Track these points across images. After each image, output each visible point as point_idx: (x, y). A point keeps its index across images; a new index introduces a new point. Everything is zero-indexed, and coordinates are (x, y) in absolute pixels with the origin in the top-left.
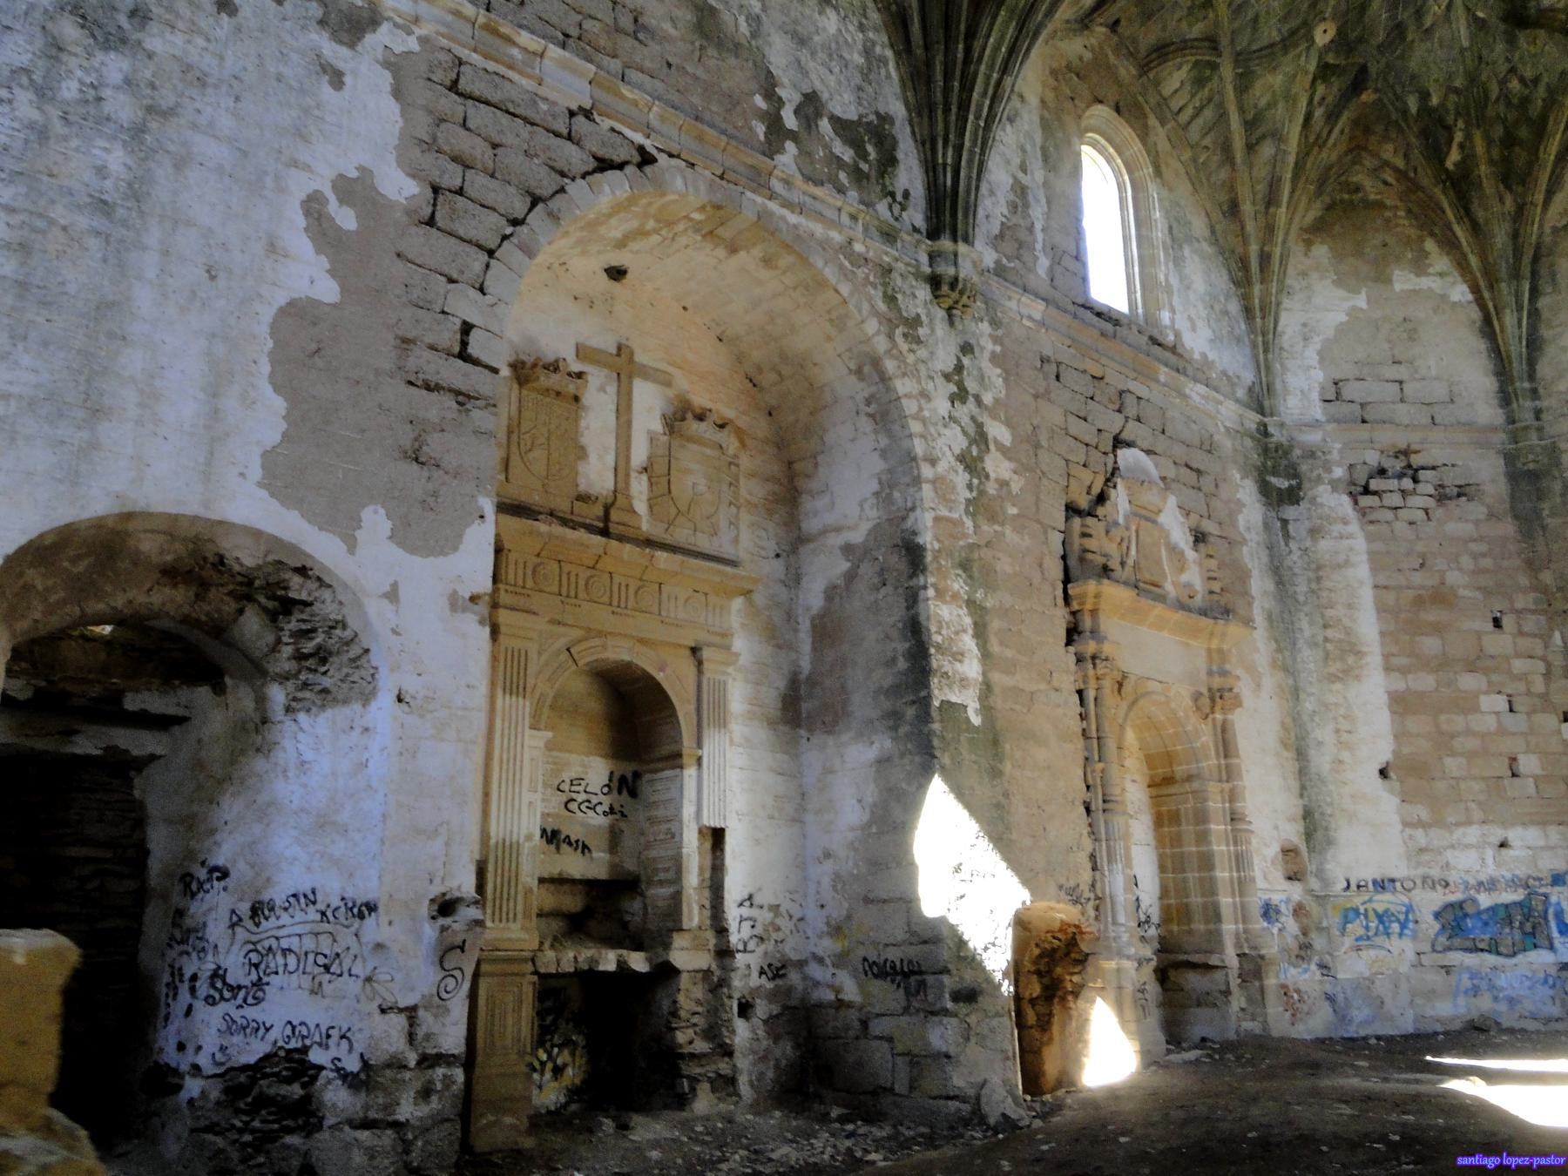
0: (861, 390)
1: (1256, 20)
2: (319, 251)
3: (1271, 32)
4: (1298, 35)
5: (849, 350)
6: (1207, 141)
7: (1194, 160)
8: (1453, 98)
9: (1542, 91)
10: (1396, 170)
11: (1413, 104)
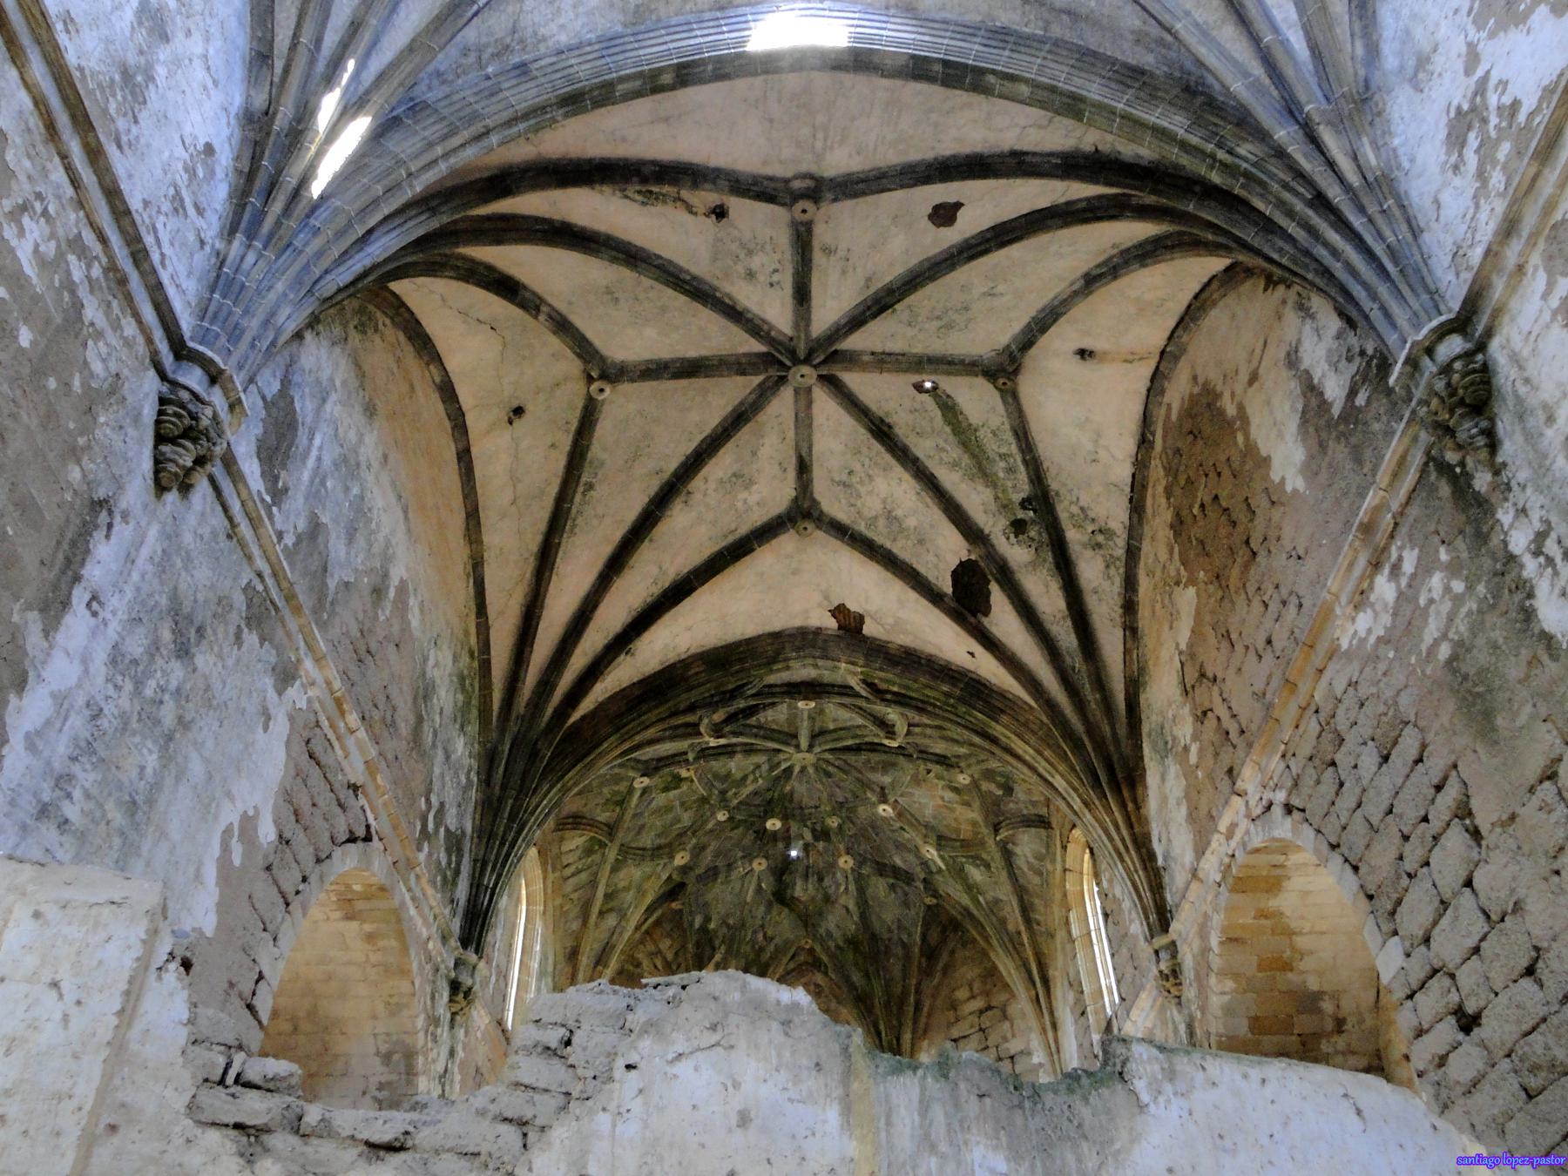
0: (379, 1072)
1: (642, 827)
2: (217, 884)
3: (647, 840)
4: (662, 851)
5: (388, 1034)
6: (575, 896)
7: (561, 906)
8: (725, 930)
9: (772, 947)
10: (665, 958)
11: (698, 921)
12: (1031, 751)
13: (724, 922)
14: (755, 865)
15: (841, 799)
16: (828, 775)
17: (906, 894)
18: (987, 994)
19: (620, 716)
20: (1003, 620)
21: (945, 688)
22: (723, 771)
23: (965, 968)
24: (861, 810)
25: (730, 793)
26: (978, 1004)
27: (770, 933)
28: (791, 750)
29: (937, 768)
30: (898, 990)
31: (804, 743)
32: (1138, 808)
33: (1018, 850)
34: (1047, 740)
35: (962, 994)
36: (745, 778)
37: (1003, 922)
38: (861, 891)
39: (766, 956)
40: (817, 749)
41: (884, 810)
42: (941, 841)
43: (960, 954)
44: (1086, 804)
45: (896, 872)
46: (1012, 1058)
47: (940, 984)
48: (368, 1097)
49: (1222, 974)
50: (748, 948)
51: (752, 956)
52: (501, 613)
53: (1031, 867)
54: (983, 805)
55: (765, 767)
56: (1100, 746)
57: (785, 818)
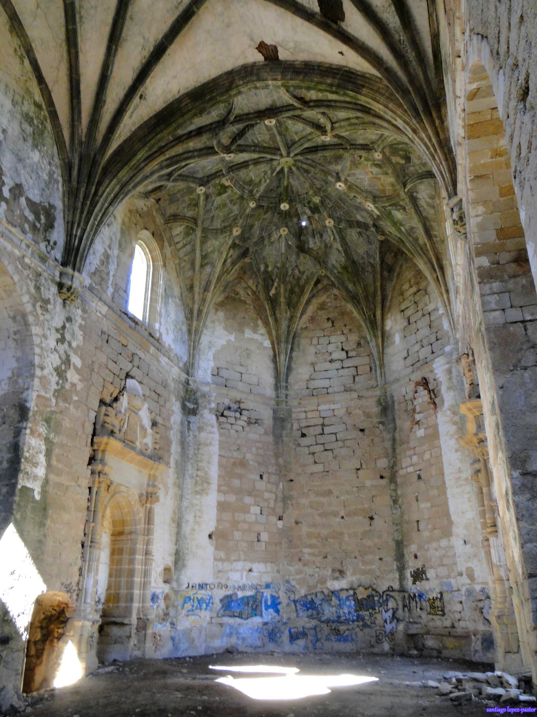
1: (213, 217)
3: (217, 224)
4: (226, 229)
5: (11, 307)
6: (186, 258)
7: (179, 264)
9: (305, 277)
11: (262, 268)
12: (381, 107)
13: (276, 266)
14: (281, 231)
15: (319, 186)
16: (307, 172)
17: (368, 237)
18: (418, 283)
19: (145, 136)
20: (355, 22)
21: (329, 81)
22: (248, 179)
23: (407, 273)
24: (330, 189)
25: (255, 191)
26: (414, 289)
27: (301, 270)
28: (278, 157)
29: (363, 153)
30: (372, 289)
31: (284, 151)
32: (442, 122)
33: (419, 196)
34: (391, 98)
35: (406, 286)
36: (261, 180)
37: (416, 240)
38: (343, 239)
39: (302, 282)
40: (292, 155)
41: (340, 186)
42: (375, 199)
43: (404, 267)
44: (414, 131)
45: (359, 224)
46: (429, 313)
47: (396, 284)
48: (11, 338)
49: (476, 202)
50: (291, 279)
51: (294, 282)
52: (56, 82)
53: (428, 205)
54: (395, 170)
55: (269, 172)
56: (419, 90)
57: (290, 202)
